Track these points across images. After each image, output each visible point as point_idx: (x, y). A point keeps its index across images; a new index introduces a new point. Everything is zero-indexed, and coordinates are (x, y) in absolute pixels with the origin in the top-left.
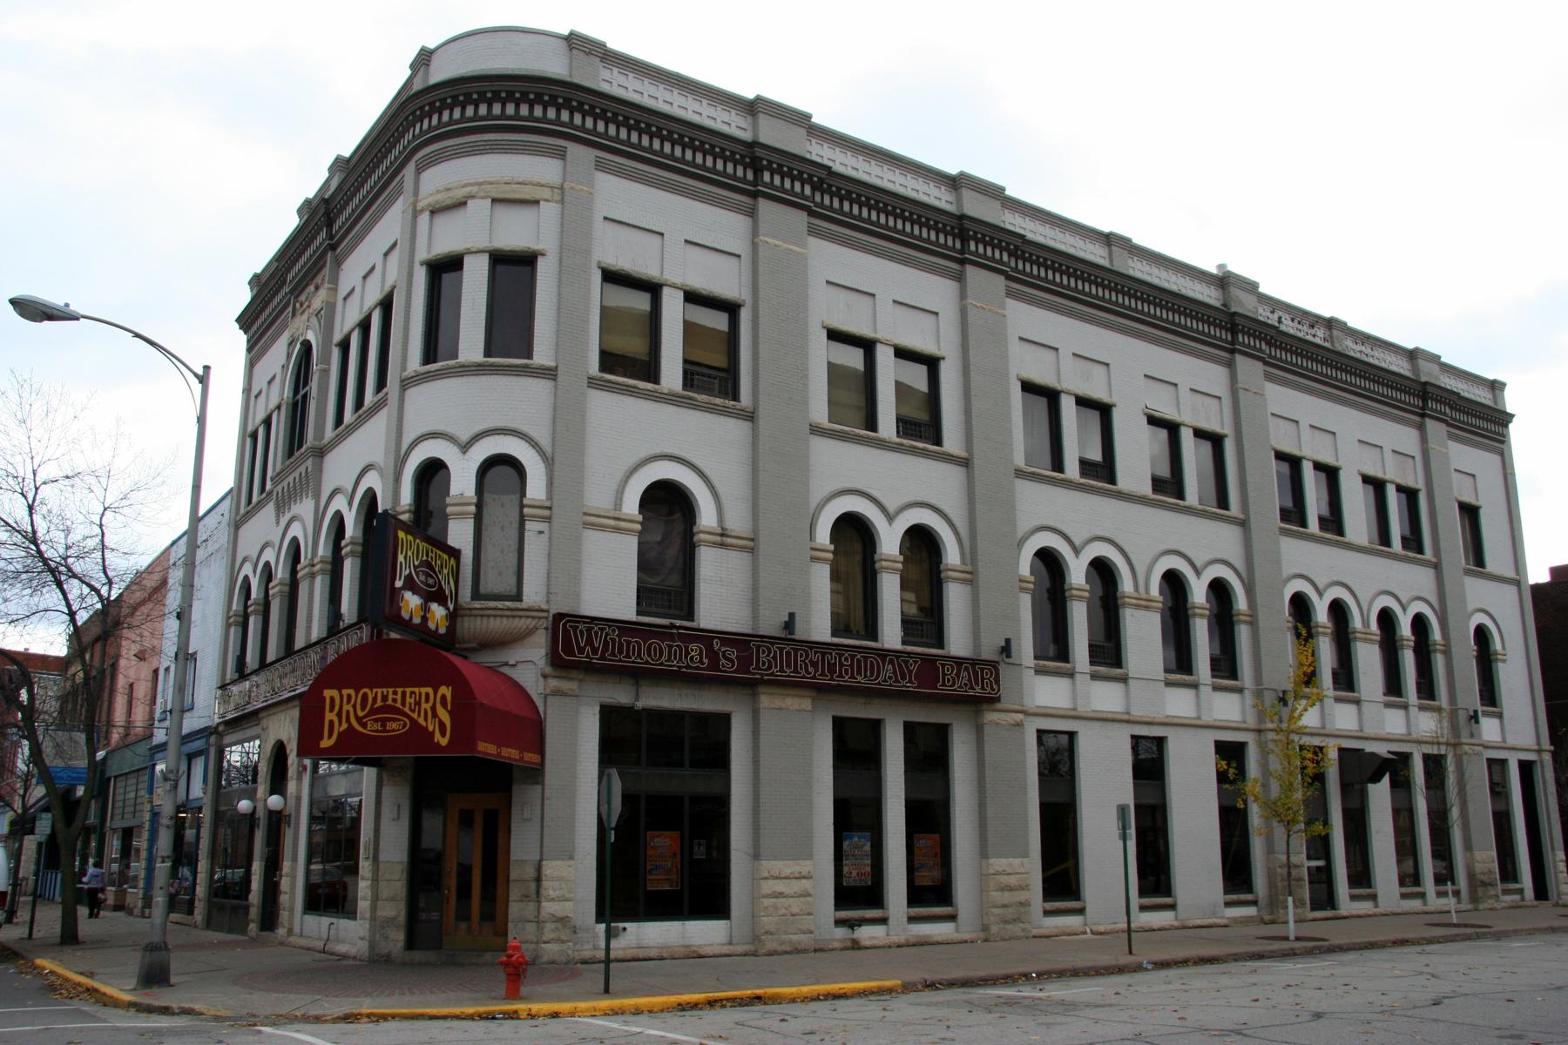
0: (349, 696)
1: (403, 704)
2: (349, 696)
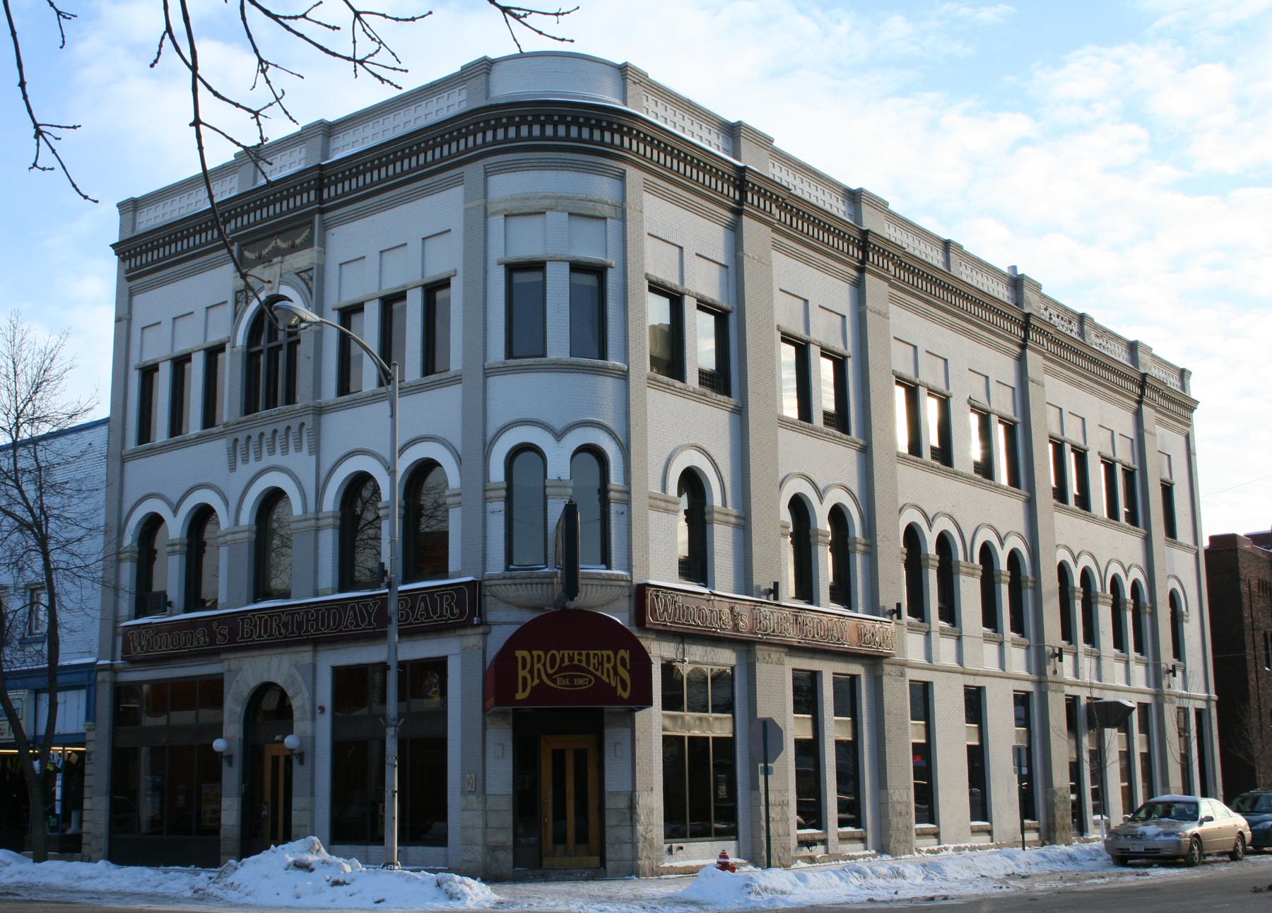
0: (539, 657)
1: (588, 664)
2: (539, 657)
